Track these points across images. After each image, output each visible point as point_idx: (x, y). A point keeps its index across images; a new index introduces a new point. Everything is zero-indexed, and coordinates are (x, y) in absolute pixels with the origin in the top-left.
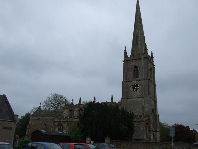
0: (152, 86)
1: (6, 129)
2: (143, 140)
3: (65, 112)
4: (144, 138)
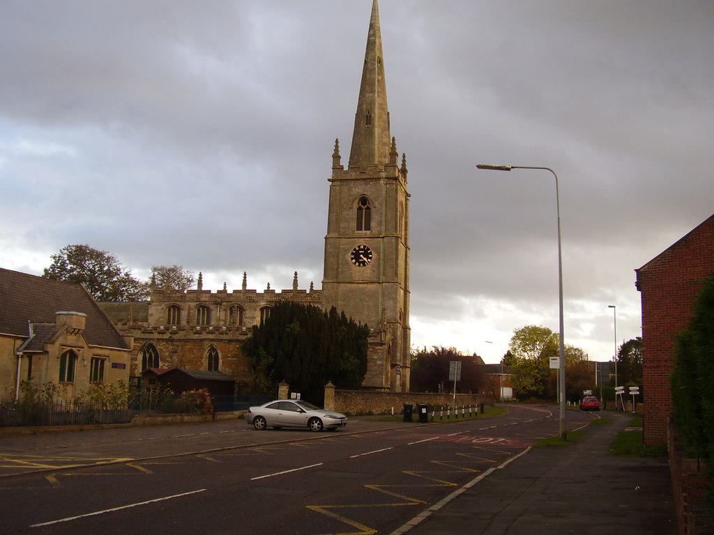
0: (401, 247)
1: (116, 367)
2: (382, 388)
3: (152, 310)
4: (384, 383)
